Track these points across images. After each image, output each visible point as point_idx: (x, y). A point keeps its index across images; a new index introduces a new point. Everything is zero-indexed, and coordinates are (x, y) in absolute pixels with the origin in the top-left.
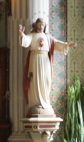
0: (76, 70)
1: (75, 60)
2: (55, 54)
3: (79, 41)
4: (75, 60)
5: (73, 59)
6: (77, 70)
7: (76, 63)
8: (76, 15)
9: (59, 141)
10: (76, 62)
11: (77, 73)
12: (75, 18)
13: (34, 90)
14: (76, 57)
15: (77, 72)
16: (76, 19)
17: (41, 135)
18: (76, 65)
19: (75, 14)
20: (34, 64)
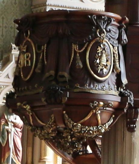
0: (4, 26)
2: (29, 128)
4: (3, 15)
10: (5, 17)
11: (6, 29)
12: (15, 6)
13: (25, 133)
14: (5, 12)
15: (6, 27)
16: (17, 7)
17: (73, 161)
18: (5, 20)
19: (15, 2)
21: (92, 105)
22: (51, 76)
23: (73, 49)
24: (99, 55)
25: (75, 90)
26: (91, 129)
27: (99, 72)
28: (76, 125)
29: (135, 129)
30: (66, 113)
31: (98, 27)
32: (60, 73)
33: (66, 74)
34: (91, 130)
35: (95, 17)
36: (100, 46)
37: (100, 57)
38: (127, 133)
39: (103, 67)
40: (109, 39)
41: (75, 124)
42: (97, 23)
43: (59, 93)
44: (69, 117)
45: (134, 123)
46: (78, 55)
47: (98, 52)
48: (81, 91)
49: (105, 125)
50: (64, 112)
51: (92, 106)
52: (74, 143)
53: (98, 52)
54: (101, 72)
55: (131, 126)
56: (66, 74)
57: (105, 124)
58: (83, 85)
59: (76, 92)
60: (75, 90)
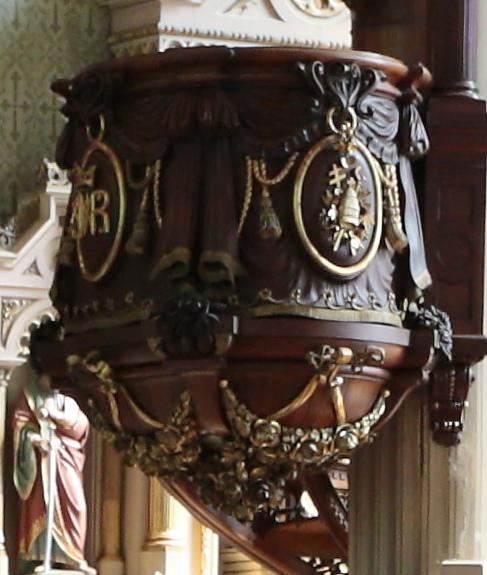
1: (16, 68)
3: (29, 113)
4: (16, 68)
5: (11, 64)
6: (25, 103)
7: (52, 27)
8: (59, 28)
9: (454, 402)
12: (55, 37)
15: (25, 107)
18: (22, 84)
20: (203, 373)
21: (316, 359)
22: (178, 264)
23: (249, 176)
24: (337, 192)
25: (260, 311)
26: (313, 436)
27: (336, 249)
28: (264, 425)
29: (460, 436)
30: (229, 386)
31: (331, 100)
32: (208, 255)
33: (228, 259)
34: (313, 441)
35: (321, 69)
36: (340, 165)
37: (340, 201)
38: (434, 450)
39: (351, 233)
40: (369, 139)
41: (260, 421)
42: (327, 88)
43: (207, 321)
44: (240, 400)
45: (456, 414)
46: (266, 194)
47: (332, 182)
48: (278, 312)
49: (358, 425)
50: (225, 383)
51: (314, 362)
52: (258, 485)
53: (332, 182)
54: (344, 250)
55: (446, 424)
56: (228, 259)
57: (360, 420)
58: (283, 293)
59: (260, 317)
60: (260, 311)
